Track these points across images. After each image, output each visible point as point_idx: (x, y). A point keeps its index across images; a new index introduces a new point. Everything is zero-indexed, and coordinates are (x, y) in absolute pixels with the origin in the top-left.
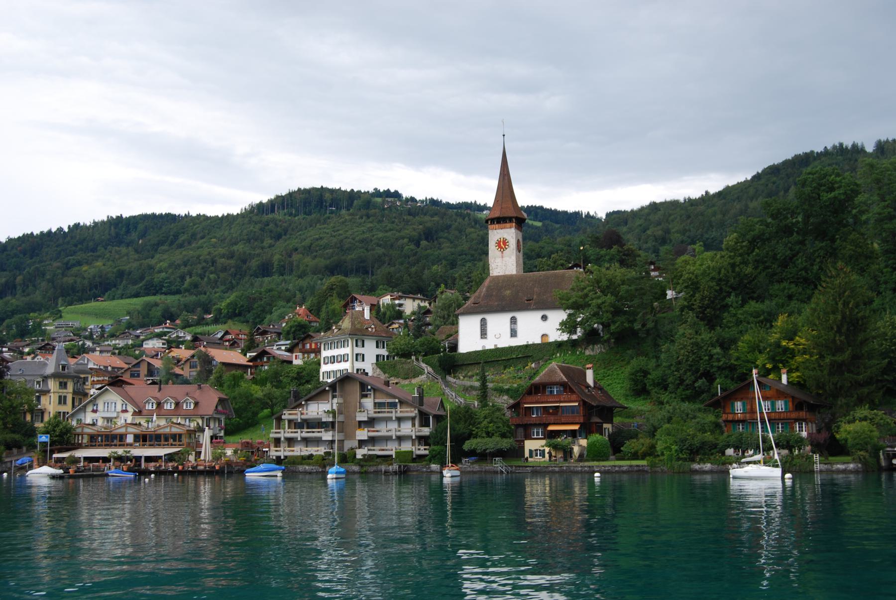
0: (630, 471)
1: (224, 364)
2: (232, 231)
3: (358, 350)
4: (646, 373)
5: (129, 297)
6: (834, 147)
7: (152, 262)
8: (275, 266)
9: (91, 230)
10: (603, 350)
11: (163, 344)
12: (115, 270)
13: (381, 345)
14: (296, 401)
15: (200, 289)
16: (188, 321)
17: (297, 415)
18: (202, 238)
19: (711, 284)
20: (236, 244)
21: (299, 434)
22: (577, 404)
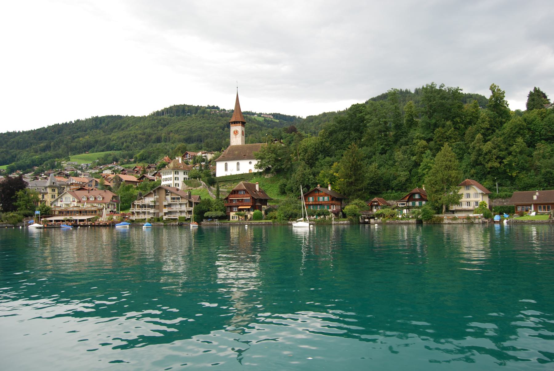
0: (265, 224)
1: (126, 181)
2: (145, 123)
3: (176, 176)
5: (100, 152)
7: (110, 136)
8: (163, 138)
9: (84, 122)
11: (112, 172)
12: (94, 140)
14: (140, 197)
15: (130, 148)
16: (123, 162)
17: (140, 203)
18: (132, 126)
19: (312, 150)
20: (146, 129)
21: (141, 210)
22: (249, 198)
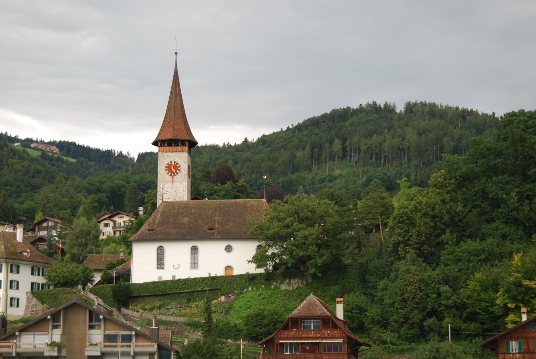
3: (13, 277)
4: (362, 310)
6: (368, 105)
10: (300, 285)
13: (36, 272)
22: (341, 341)
